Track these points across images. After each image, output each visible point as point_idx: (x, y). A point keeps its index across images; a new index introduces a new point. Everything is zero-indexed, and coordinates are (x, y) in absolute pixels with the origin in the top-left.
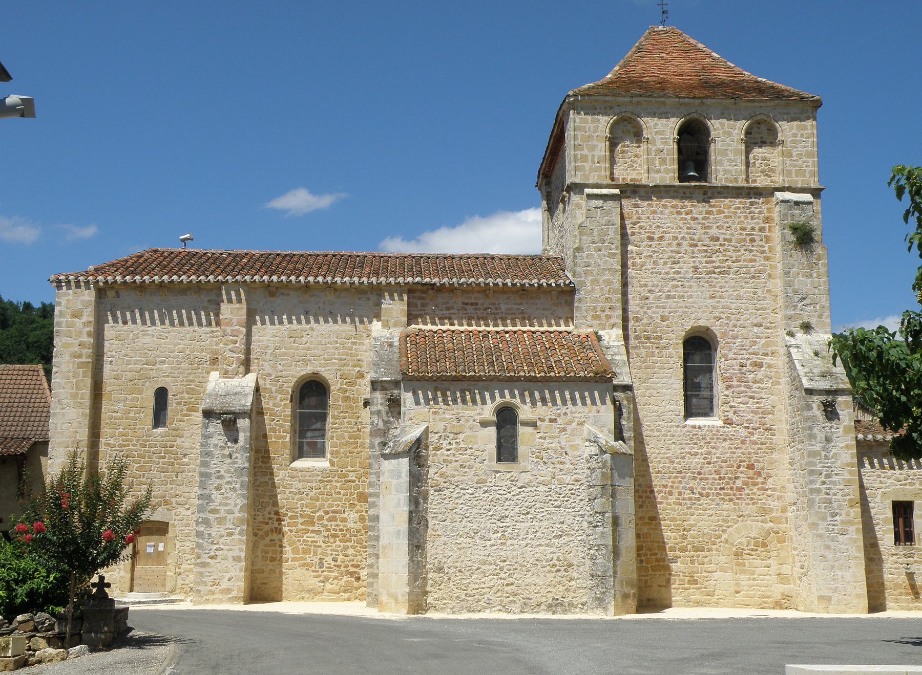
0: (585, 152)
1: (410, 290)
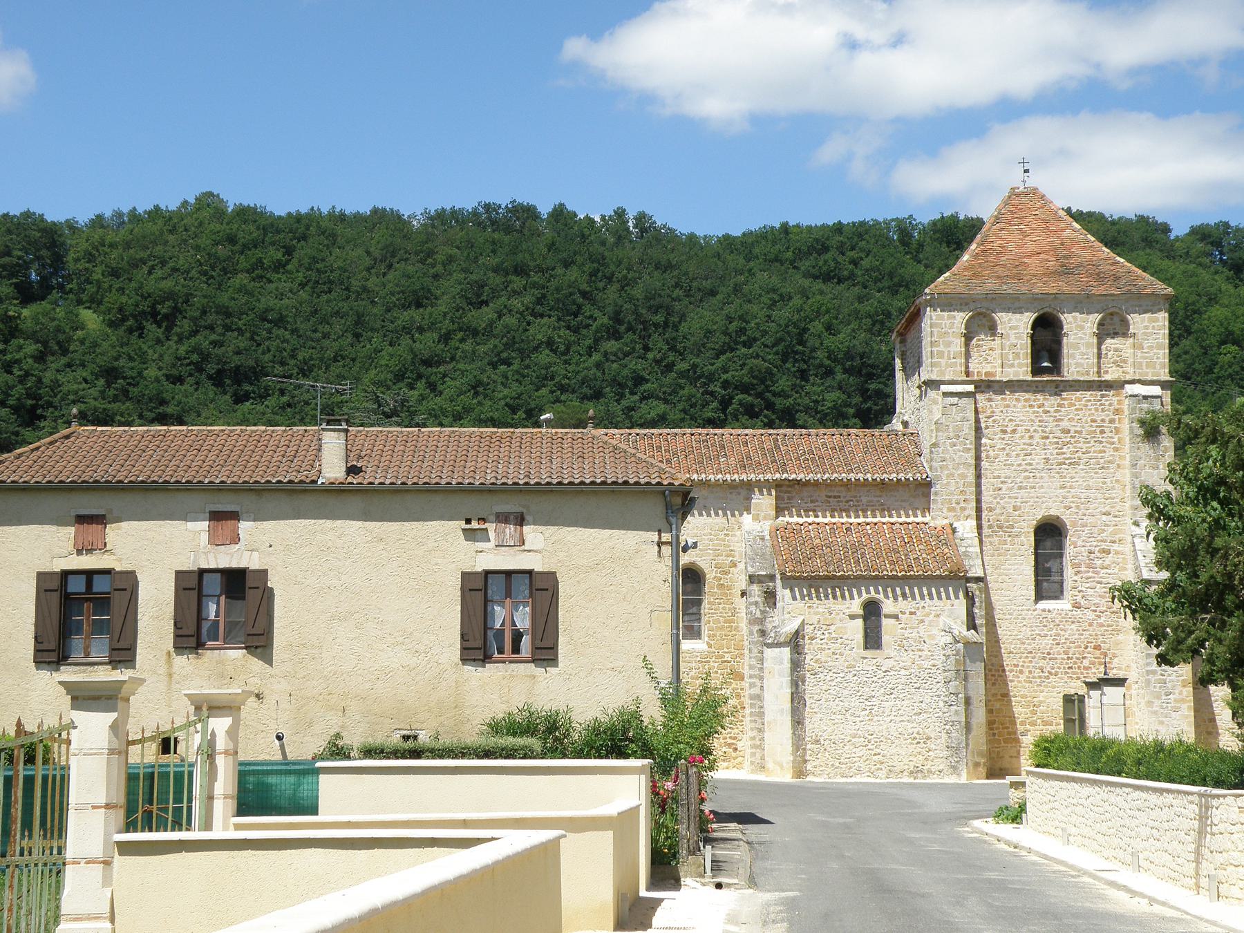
0: (942, 348)
1: (778, 485)
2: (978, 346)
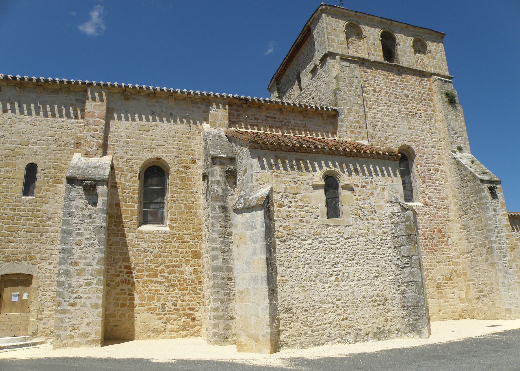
0: (333, 37)
2: (352, 43)
